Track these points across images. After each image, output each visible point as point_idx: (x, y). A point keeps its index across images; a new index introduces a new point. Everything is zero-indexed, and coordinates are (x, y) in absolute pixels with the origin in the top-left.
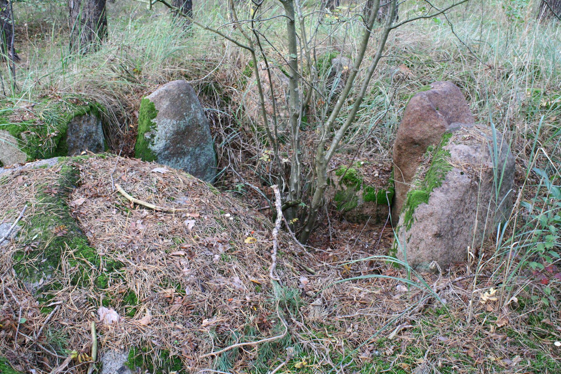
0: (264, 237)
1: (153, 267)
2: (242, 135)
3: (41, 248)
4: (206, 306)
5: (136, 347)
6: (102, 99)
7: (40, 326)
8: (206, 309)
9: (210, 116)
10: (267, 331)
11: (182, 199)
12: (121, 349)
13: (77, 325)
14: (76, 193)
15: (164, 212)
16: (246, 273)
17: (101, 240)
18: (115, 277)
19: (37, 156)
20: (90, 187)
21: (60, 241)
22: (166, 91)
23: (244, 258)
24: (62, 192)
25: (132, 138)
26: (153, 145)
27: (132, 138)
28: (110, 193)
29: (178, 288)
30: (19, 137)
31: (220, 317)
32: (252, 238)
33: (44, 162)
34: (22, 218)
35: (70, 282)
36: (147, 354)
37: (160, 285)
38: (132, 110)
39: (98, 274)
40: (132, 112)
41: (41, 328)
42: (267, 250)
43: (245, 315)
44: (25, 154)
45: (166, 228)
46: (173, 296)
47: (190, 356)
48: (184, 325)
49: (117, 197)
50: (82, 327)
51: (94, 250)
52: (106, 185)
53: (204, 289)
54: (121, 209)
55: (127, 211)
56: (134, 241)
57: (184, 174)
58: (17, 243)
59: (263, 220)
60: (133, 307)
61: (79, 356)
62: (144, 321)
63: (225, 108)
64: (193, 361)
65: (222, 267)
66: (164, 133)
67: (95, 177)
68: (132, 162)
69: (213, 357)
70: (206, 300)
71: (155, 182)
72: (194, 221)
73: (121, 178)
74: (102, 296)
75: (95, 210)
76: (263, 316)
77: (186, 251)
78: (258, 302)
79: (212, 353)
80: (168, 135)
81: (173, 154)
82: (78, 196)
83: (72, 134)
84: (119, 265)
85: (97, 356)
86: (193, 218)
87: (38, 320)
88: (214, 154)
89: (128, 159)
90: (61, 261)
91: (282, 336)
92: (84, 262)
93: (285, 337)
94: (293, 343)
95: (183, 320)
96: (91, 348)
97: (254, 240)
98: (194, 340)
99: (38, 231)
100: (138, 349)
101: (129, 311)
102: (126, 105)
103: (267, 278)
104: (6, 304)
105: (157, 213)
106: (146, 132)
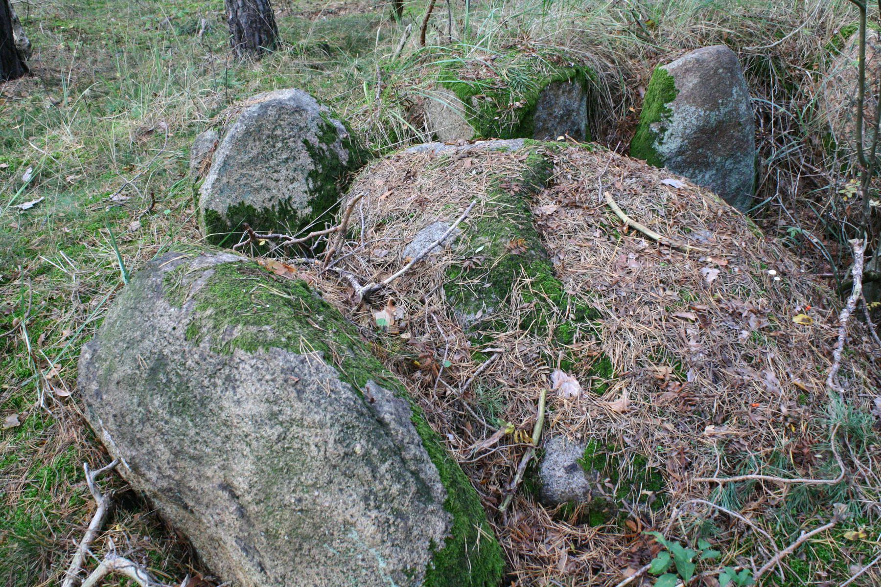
0: (825, 320)
1: (643, 329)
2: (805, 151)
3: (486, 267)
4: (715, 405)
5: (599, 440)
6: (593, 61)
7: (469, 378)
8: (714, 411)
9: (758, 111)
10: (806, 468)
11: (703, 233)
12: (577, 439)
13: (519, 388)
14: (545, 195)
15: (673, 248)
16: (788, 370)
17: (573, 273)
18: (585, 331)
19: (487, 135)
20: (566, 190)
21: (514, 262)
22: (697, 61)
23: (789, 345)
24: (525, 190)
25: (630, 128)
26: (661, 143)
27: (630, 128)
28: (594, 204)
29: (678, 368)
30: (468, 101)
31: (734, 427)
32: (805, 316)
33: (503, 143)
34: (466, 217)
35: (518, 323)
36: (613, 454)
37: (651, 357)
38: (636, 84)
39: (560, 321)
40: (636, 87)
41: (470, 380)
42: (826, 341)
43: (775, 434)
44: (473, 128)
45: (672, 273)
46: (667, 378)
47: (677, 475)
48: (676, 425)
49: (604, 213)
50: (526, 392)
51: (561, 284)
52: (590, 191)
53: (716, 379)
54: (608, 231)
55: (617, 237)
56: (621, 284)
57: (711, 195)
58: (453, 252)
59: (826, 292)
60: (604, 381)
61: (516, 432)
62: (617, 405)
63: (784, 101)
64: (680, 484)
65: (751, 352)
66: (681, 127)
67: (575, 177)
68: (631, 163)
69: (713, 485)
70: (717, 397)
71: (665, 200)
72: (717, 271)
73: (613, 184)
74: (561, 354)
75: (569, 226)
76: (805, 443)
77: (698, 315)
78: (799, 419)
79: (715, 479)
80: (688, 131)
81: (689, 163)
82: (547, 200)
83: (544, 108)
84: (594, 315)
85: (540, 440)
86: (717, 267)
87: (467, 368)
88: (753, 174)
89: (627, 158)
90: (511, 291)
91: (834, 481)
92: (544, 300)
93: (837, 484)
94: (847, 498)
95: (676, 418)
96: (534, 425)
97: (809, 321)
98: (687, 453)
99: (485, 241)
100: (602, 444)
101: (598, 386)
102: (628, 75)
103: (820, 385)
104: (427, 335)
105: (662, 248)
106: (653, 121)
